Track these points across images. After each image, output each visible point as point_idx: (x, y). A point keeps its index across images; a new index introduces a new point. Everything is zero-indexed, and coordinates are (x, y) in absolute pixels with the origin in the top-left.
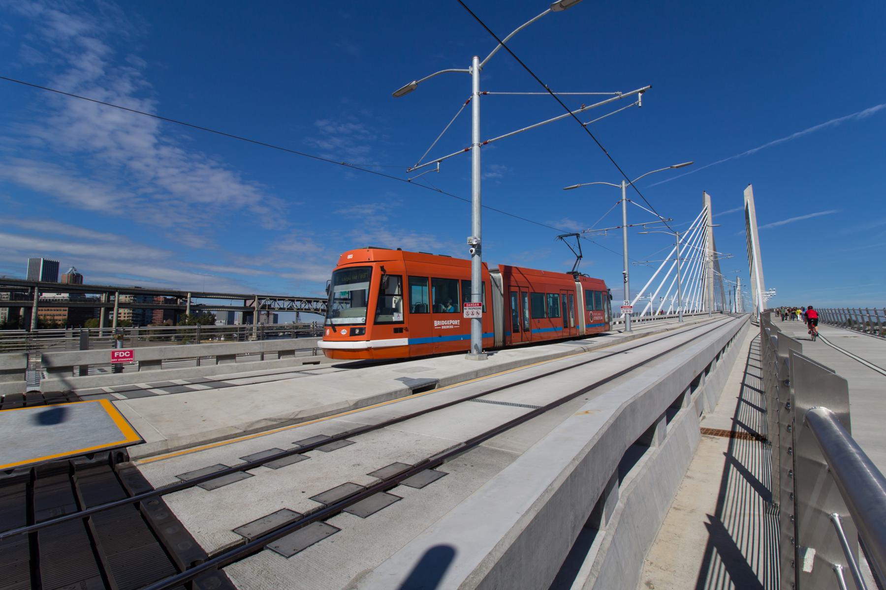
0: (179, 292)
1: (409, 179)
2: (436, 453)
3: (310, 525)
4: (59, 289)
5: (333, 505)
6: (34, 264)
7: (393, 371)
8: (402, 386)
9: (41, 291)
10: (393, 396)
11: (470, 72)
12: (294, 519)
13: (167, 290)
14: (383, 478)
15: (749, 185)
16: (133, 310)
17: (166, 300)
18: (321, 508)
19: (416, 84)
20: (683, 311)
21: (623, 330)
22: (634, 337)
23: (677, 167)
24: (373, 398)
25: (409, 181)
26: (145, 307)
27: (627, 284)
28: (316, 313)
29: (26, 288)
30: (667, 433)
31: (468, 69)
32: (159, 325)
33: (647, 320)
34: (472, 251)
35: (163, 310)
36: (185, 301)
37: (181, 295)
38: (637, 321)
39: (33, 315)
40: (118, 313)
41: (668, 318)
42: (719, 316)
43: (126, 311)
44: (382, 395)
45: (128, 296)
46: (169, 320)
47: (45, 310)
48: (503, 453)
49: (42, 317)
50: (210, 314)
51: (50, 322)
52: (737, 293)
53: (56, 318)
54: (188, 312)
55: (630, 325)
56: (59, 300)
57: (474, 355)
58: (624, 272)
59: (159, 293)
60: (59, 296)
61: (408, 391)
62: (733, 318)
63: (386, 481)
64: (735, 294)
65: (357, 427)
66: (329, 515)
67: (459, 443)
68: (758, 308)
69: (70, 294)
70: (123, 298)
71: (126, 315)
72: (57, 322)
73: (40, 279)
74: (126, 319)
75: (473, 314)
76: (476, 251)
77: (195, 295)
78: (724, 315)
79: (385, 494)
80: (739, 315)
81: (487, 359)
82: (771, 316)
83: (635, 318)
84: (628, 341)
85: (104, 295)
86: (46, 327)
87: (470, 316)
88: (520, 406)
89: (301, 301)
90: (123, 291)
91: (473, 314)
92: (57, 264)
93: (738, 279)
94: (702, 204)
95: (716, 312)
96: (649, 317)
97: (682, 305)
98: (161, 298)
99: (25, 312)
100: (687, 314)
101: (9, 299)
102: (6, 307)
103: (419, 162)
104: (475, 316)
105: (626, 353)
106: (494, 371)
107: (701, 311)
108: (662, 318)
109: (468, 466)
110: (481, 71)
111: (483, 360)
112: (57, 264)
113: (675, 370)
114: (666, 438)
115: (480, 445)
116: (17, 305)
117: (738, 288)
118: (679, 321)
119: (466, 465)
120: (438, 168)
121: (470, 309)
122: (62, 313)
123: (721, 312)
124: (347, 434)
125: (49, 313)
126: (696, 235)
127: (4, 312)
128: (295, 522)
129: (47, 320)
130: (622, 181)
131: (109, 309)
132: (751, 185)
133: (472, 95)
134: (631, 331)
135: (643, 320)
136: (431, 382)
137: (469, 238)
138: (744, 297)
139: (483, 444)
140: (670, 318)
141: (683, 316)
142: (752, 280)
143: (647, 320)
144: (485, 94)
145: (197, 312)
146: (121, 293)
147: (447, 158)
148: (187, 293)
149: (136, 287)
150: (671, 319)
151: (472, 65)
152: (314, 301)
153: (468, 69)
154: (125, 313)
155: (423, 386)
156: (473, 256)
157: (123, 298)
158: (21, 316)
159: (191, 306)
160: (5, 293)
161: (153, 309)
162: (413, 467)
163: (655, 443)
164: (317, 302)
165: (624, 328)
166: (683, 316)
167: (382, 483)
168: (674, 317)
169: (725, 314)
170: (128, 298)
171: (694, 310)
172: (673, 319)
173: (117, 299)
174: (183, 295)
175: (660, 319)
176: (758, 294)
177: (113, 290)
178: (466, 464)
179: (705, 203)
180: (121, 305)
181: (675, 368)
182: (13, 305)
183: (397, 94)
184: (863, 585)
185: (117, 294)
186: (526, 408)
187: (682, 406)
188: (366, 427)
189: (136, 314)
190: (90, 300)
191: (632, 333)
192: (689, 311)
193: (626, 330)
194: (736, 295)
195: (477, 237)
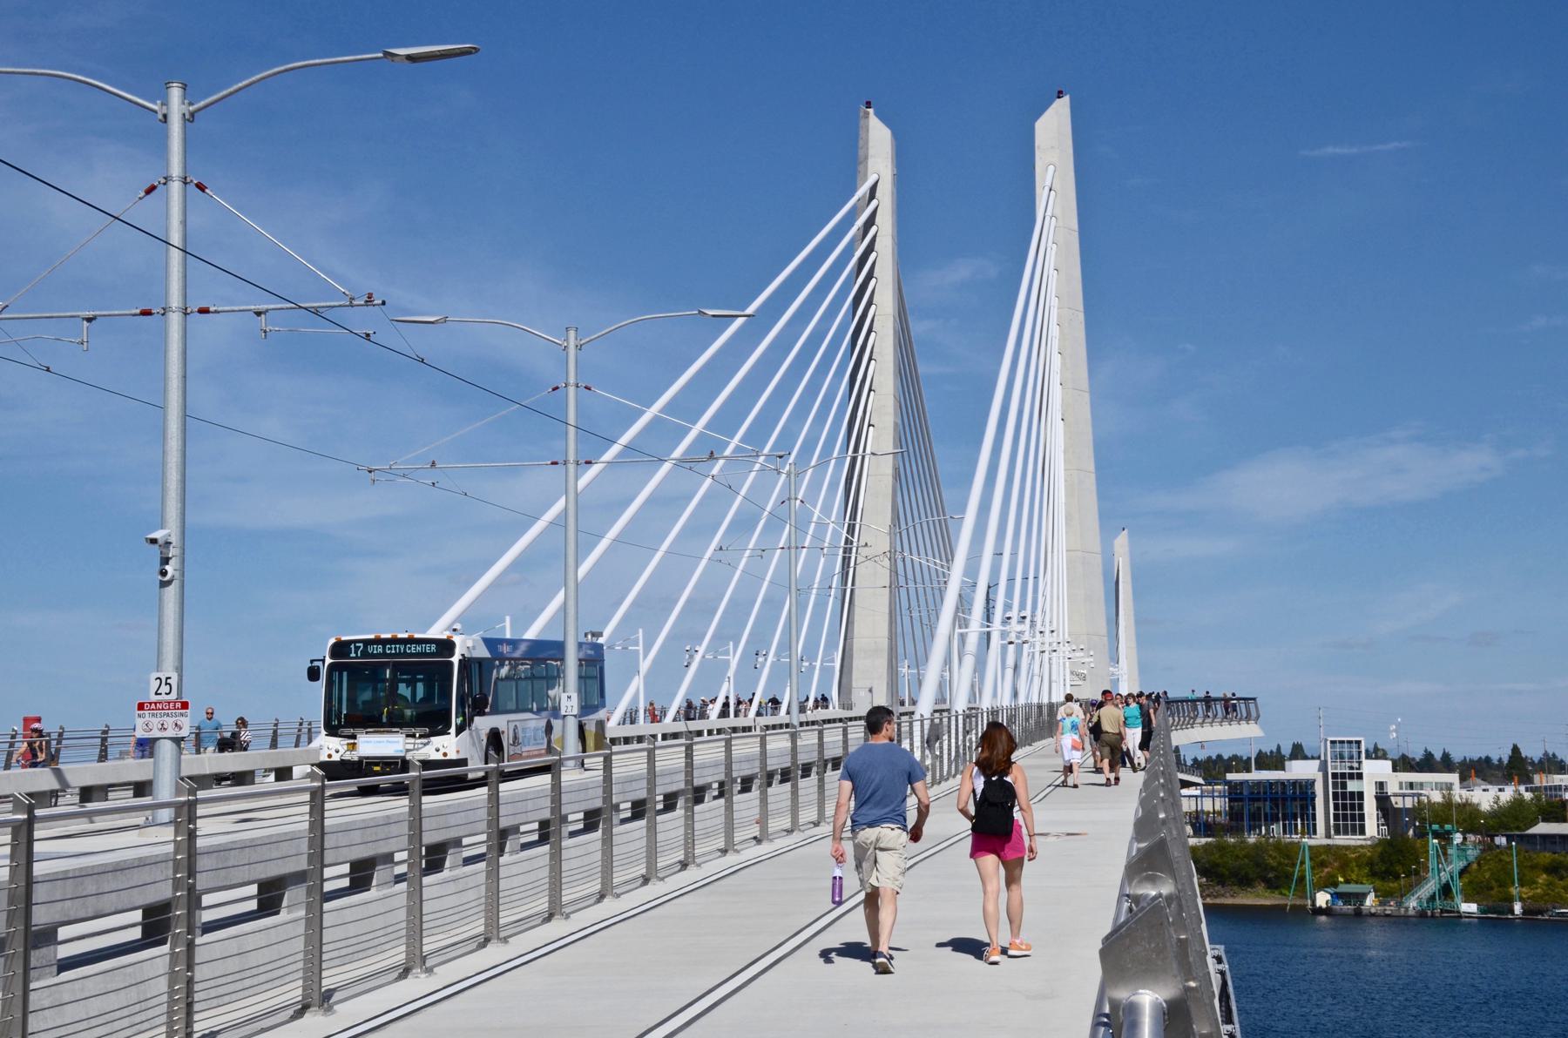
15: (1060, 95)
23: (410, 58)
27: (171, 592)
130: (167, 86)
132: (1066, 99)
179: (871, 162)
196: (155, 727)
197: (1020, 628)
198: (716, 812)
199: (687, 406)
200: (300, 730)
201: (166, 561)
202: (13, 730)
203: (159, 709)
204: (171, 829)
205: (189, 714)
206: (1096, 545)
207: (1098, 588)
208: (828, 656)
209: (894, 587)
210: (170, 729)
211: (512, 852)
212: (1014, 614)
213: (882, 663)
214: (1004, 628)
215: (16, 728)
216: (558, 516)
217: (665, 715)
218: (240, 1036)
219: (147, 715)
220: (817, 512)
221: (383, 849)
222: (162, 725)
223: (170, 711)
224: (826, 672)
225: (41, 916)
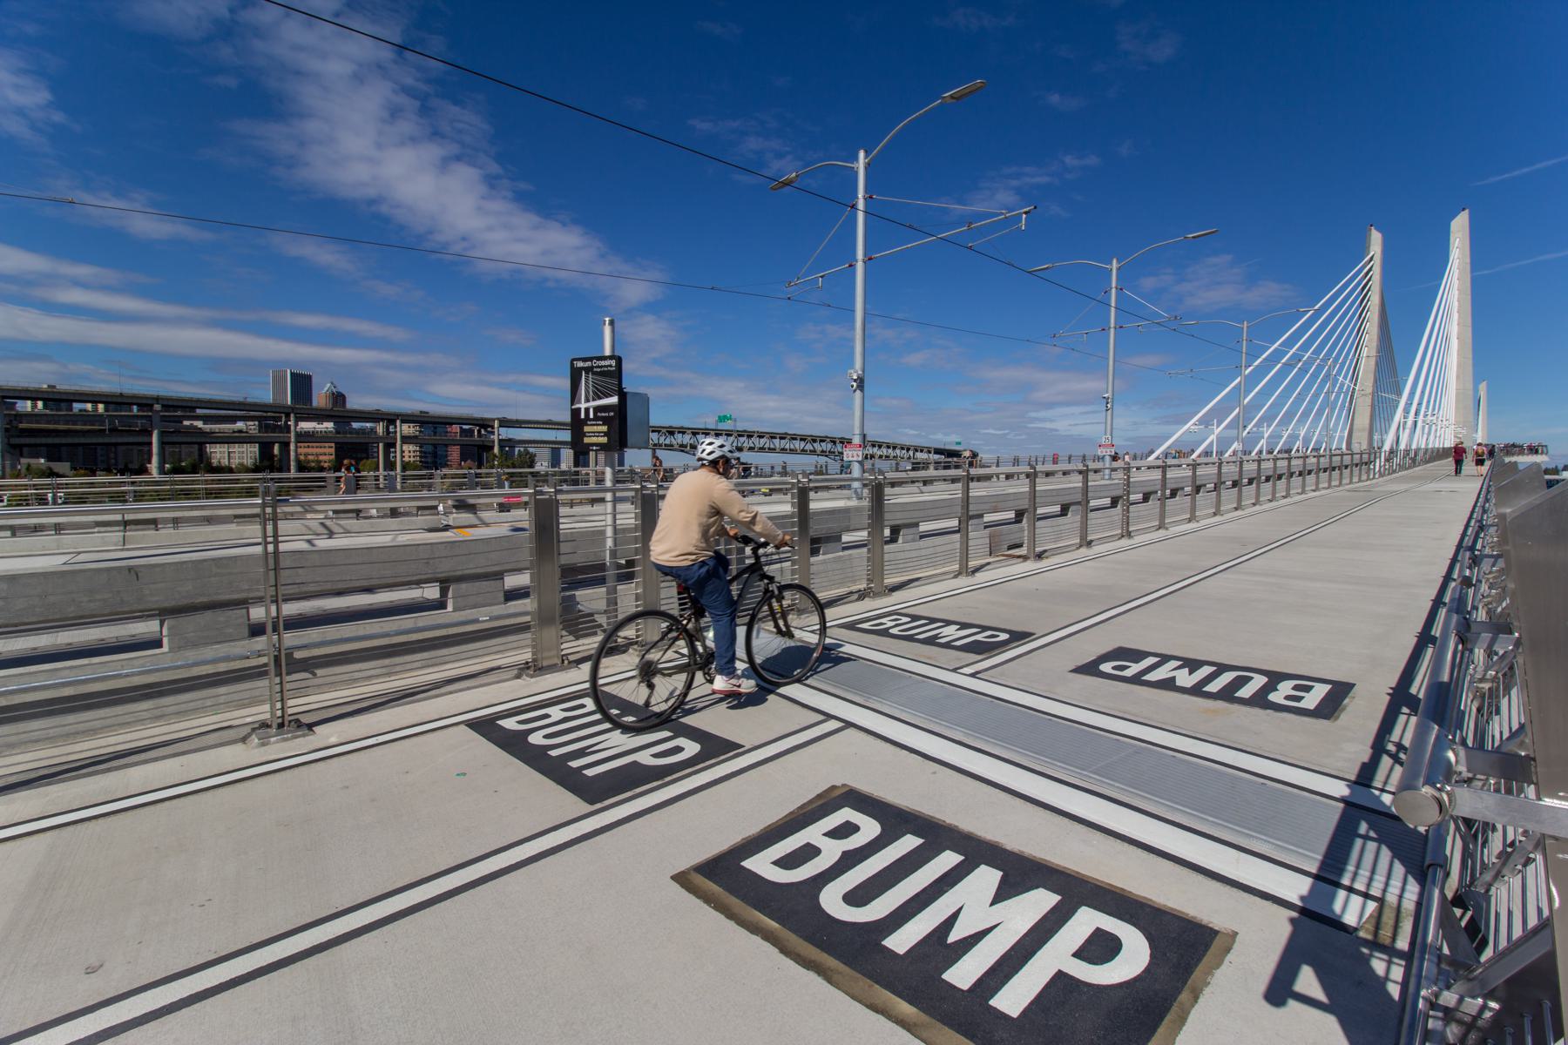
0: (482, 419)
4: (319, 416)
6: (278, 380)
9: (297, 420)
13: (465, 416)
15: (1463, 210)
16: (420, 447)
17: (462, 430)
25: (789, 299)
26: (436, 442)
28: (682, 451)
29: (278, 415)
32: (457, 469)
34: (852, 386)
35: (458, 447)
36: (489, 432)
37: (485, 424)
39: (292, 454)
40: (403, 452)
43: (412, 447)
45: (412, 425)
46: (469, 461)
47: (305, 447)
49: (302, 457)
50: (528, 453)
51: (313, 464)
53: (321, 458)
54: (496, 450)
56: (321, 432)
58: (1106, 396)
59: (454, 421)
60: (321, 426)
69: (335, 423)
70: (407, 429)
71: (412, 454)
72: (322, 464)
73: (289, 403)
74: (412, 459)
76: (858, 386)
77: (505, 423)
85: (381, 423)
86: (310, 470)
87: (851, 459)
89: (659, 432)
90: (407, 419)
91: (853, 457)
92: (309, 377)
94: (1363, 247)
98: (456, 428)
99: (281, 450)
101: (257, 431)
102: (256, 443)
104: (855, 459)
110: (868, 166)
112: (309, 377)
116: (269, 440)
122: (327, 450)
125: (310, 451)
126: (1350, 310)
127: (252, 449)
129: (309, 462)
130: (1112, 260)
131: (390, 445)
132: (1467, 211)
133: (857, 198)
137: (849, 371)
144: (871, 197)
145: (507, 449)
146: (403, 422)
148: (494, 420)
149: (421, 412)
152: (679, 432)
153: (853, 163)
154: (410, 452)
156: (855, 391)
157: (407, 429)
158: (276, 456)
159: (500, 441)
160: (252, 423)
161: (446, 445)
164: (684, 433)
170: (412, 429)
173: (398, 429)
174: (488, 423)
177: (392, 418)
180: (406, 439)
182: (265, 440)
185: (398, 422)
189: (425, 453)
190: (358, 432)
197: (1431, 418)
198: (1075, 525)
199: (1290, 343)
201: (1107, 403)
204: (790, 505)
206: (1470, 385)
207: (1470, 403)
208: (1342, 431)
209: (1373, 406)
211: (1203, 492)
212: (1429, 413)
213: (1365, 435)
216: (1237, 385)
220: (1341, 379)
221: (1181, 485)
224: (1341, 438)
225: (1223, 480)
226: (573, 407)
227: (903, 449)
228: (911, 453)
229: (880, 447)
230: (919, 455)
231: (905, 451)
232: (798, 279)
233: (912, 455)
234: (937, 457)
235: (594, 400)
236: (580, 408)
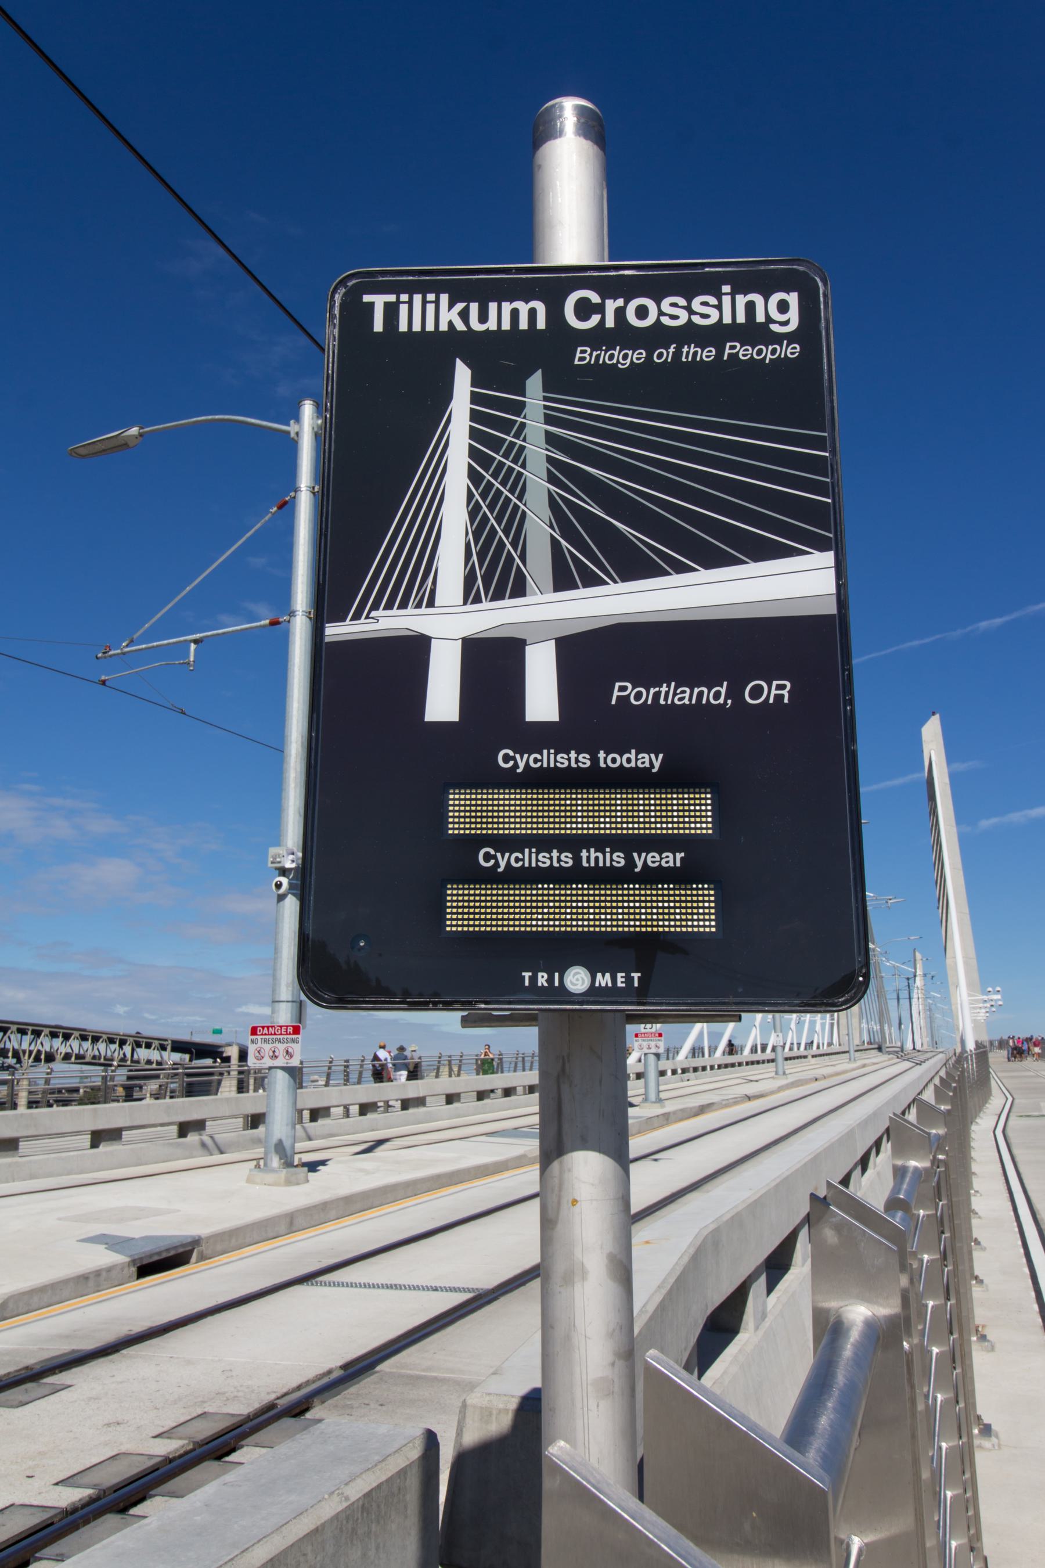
1: (103, 678)
2: (285, 1390)
3: (92, 1524)
5: (115, 1491)
7: (60, 1219)
8: (105, 1258)
10: (91, 1283)
11: (293, 435)
12: (51, 1517)
14: (195, 1440)
15: (934, 714)
18: (94, 1497)
19: (141, 435)
20: (783, 1047)
21: (640, 1099)
22: (667, 1119)
24: (42, 1290)
25: (104, 683)
30: (768, 1309)
31: (288, 425)
33: (695, 1070)
34: (279, 886)
38: (669, 1073)
41: (747, 1064)
42: (875, 1057)
44: (66, 1282)
48: (435, 1379)
52: (915, 996)
55: (658, 1085)
57: (273, 1171)
61: (126, 1270)
62: (907, 1065)
63: (203, 1445)
64: (910, 998)
65: (46, 1355)
66: (122, 1504)
67: (328, 1369)
68: (963, 1042)
75: (274, 1057)
78: (886, 1057)
79: (221, 1463)
80: (922, 1057)
81: (308, 1181)
82: (990, 1060)
83: (666, 1065)
84: (654, 1129)
87: (267, 1062)
88: (436, 1289)
91: (274, 1057)
93: (918, 956)
95: (866, 1046)
96: (698, 1062)
97: (781, 1032)
100: (795, 1052)
103: (135, 636)
104: (281, 1062)
105: (656, 1160)
106: (333, 1214)
107: (830, 1044)
108: (733, 1065)
109: (372, 1406)
111: (298, 1184)
113: (778, 1181)
114: (767, 1320)
115: (378, 1368)
117: (919, 981)
118: (777, 1073)
119: (368, 1404)
120: (192, 659)
121: (266, 1041)
123: (880, 1049)
124: (30, 1373)
128: (52, 1524)
133: (296, 490)
134: (659, 1100)
135: (684, 1071)
136: (183, 1245)
137: (273, 851)
138: (933, 1007)
139: (385, 1367)
140: (753, 1063)
141: (786, 1059)
142: (949, 961)
143: (695, 1070)
147: (218, 635)
150: (755, 1066)
151: (297, 418)
153: (288, 425)
155: (164, 1255)
156: (281, 898)
162: (249, 1418)
163: (747, 1324)
165: (642, 1091)
166: (786, 1059)
167: (193, 1450)
168: (763, 1062)
169: (889, 1053)
171: (812, 1042)
172: (761, 1066)
175: (726, 1066)
176: (961, 1001)
178: (366, 1402)
181: (778, 1177)
183: (83, 451)
184: (335, 360)
186: (456, 1294)
187: (793, 1263)
188: (148, 1329)
191: (663, 1107)
192: (799, 1044)
193: (646, 1100)
194: (914, 1001)
195: (295, 850)
196: (267, 1054)
200: (362, 1066)
202: (331, 1058)
203: (271, 1034)
205: (300, 1040)
210: (281, 1057)
214: (43, 1061)
215: (332, 1056)
217: (678, 1053)
218: (263, 1553)
219: (260, 1041)
222: (274, 1052)
223: (281, 1037)
226: (334, 631)
227: (111, 1041)
228: (128, 1049)
229: (67, 1037)
230: (143, 1054)
231: (116, 1046)
232: (131, 642)
233: (129, 1055)
234: (177, 1057)
235: (563, 581)
236: (470, 595)
